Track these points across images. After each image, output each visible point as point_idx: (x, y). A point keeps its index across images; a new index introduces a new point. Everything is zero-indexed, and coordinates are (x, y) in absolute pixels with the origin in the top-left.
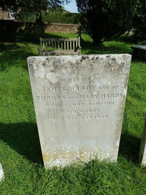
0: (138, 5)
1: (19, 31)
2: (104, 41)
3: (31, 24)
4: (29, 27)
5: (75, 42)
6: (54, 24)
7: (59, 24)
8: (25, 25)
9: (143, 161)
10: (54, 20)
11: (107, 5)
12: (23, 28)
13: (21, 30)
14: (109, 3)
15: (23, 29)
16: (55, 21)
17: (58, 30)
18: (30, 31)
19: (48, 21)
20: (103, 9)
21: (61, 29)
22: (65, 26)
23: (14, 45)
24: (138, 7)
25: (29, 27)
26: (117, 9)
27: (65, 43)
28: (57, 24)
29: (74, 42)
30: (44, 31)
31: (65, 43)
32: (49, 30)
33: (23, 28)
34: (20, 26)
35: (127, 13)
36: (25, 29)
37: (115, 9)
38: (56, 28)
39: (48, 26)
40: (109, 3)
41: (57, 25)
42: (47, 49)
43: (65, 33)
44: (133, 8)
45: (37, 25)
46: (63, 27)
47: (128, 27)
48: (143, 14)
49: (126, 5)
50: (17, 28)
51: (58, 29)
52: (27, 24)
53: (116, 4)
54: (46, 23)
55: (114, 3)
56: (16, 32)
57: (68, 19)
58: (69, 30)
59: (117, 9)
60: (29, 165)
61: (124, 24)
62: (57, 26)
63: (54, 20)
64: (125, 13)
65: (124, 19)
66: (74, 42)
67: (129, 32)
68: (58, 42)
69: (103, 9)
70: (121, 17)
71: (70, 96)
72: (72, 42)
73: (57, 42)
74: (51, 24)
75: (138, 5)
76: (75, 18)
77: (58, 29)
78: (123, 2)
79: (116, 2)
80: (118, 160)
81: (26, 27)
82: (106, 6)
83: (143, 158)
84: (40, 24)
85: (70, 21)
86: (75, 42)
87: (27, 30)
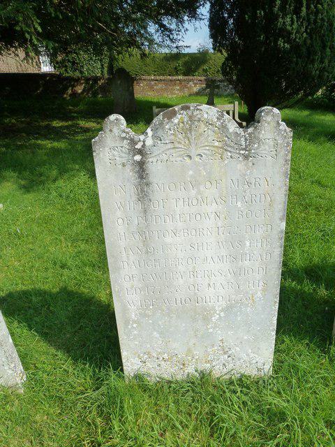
1: (70, 95)
3: (96, 79)
4: (92, 87)
6: (148, 78)
7: (158, 78)
8: (82, 84)
11: (290, 33)
12: (79, 89)
13: (74, 94)
14: (292, 29)
15: (80, 91)
18: (95, 94)
20: (281, 43)
23: (76, 126)
25: (92, 87)
26: (309, 42)
30: (132, 94)
33: (79, 89)
34: (73, 86)
35: (328, 50)
36: (84, 90)
37: (305, 41)
38: (151, 88)
40: (292, 29)
45: (119, 82)
50: (66, 89)
52: (87, 80)
53: (306, 31)
55: (303, 30)
56: (65, 99)
57: (174, 64)
58: (180, 90)
59: (309, 42)
60: (76, 376)
61: (323, 70)
62: (153, 83)
64: (324, 47)
65: (322, 62)
69: (281, 43)
71: (234, 179)
76: (185, 64)
80: (278, 365)
81: (85, 87)
84: (125, 78)
85: (176, 71)
87: (87, 94)
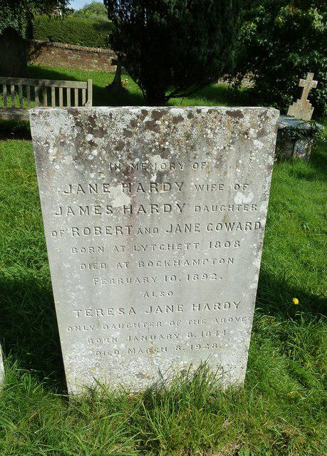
0: (262, 16)
2: (172, 96)
5: (80, 91)
6: (61, 45)
7: (78, 47)
9: (68, 385)
10: (65, 35)
16: (67, 39)
17: (70, 60)
19: (50, 38)
21: (77, 60)
22: (88, 52)
24: (261, 21)
27: (53, 94)
28: (67, 46)
29: (69, 92)
31: (53, 94)
32: (46, 60)
38: (65, 57)
39: (44, 49)
41: (66, 49)
42: (5, 105)
43: (86, 69)
44: (235, 21)
45: (8, 44)
46: (82, 56)
47: (224, 65)
48: (273, 40)
49: (215, 14)
51: (69, 58)
54: (39, 41)
61: (211, 57)
62: (67, 52)
63: (65, 35)
64: (212, 30)
65: (210, 46)
66: (69, 92)
67: (241, 79)
68: (36, 89)
70: (203, 40)
72: (72, 90)
73: (32, 88)
74: (52, 46)
75: (262, 16)
77: (69, 58)
78: (207, 4)
79: (189, 3)
82: (163, 9)
83: (67, 377)
86: (80, 91)
